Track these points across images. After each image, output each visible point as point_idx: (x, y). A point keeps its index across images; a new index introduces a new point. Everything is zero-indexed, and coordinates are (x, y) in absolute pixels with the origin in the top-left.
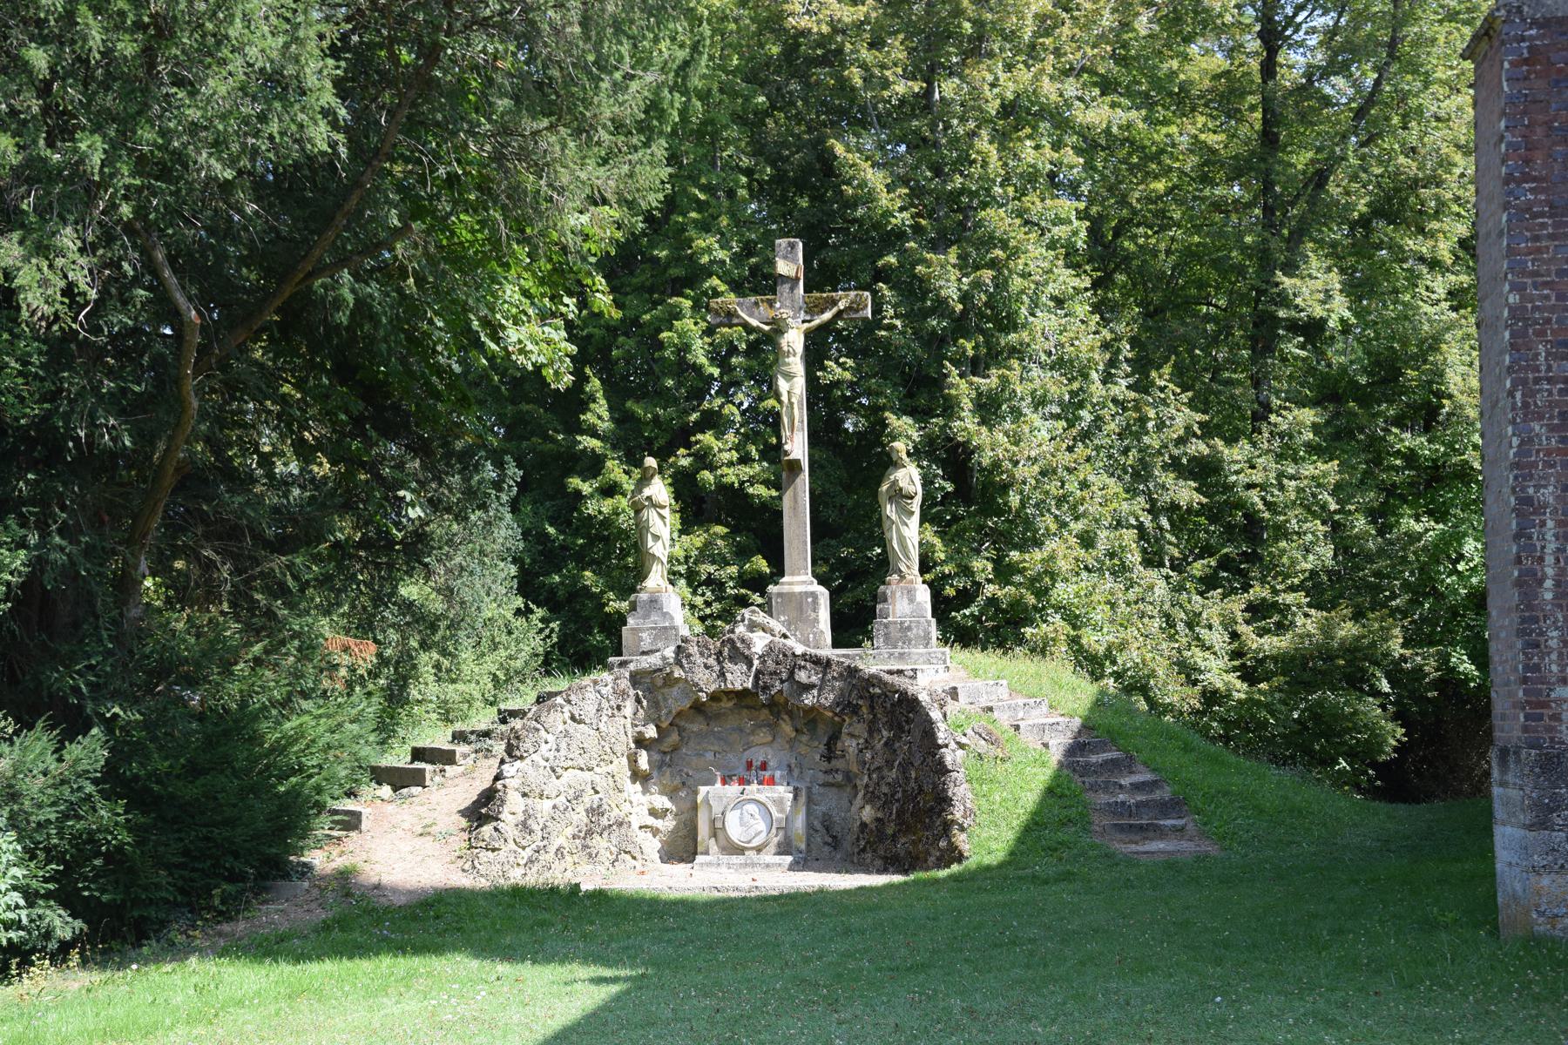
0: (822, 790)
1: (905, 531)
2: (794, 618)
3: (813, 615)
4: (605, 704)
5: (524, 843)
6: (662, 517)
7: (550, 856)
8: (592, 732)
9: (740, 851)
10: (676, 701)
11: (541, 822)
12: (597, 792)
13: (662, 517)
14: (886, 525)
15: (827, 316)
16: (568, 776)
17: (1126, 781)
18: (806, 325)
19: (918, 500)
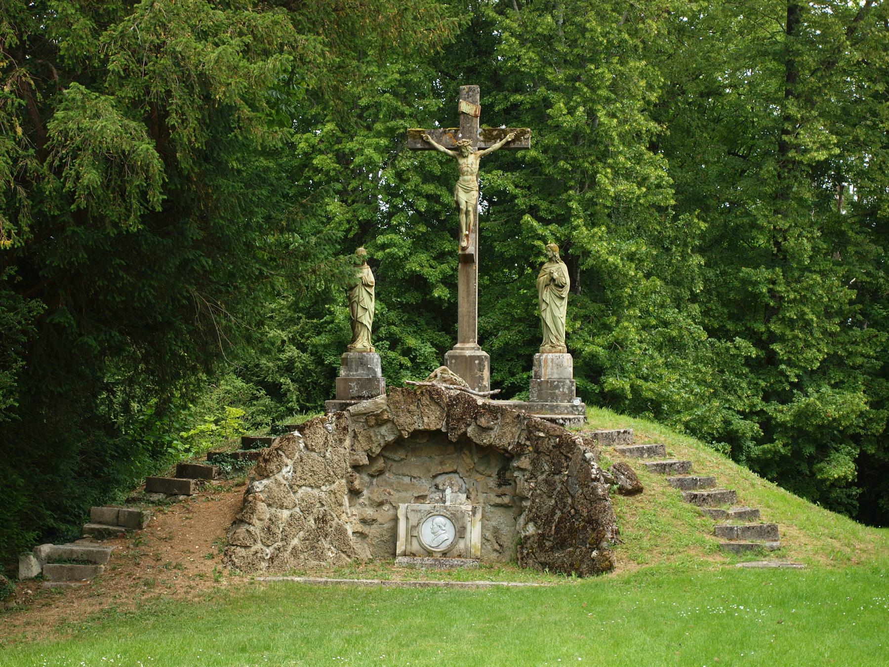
0: (493, 509)
1: (557, 314)
3: (479, 374)
4: (330, 438)
5: (268, 542)
7: (287, 554)
8: (320, 459)
9: (430, 553)
10: (387, 434)
11: (281, 526)
12: (323, 505)
14: (544, 306)
15: (497, 145)
16: (301, 492)
18: (482, 152)
19: (568, 288)
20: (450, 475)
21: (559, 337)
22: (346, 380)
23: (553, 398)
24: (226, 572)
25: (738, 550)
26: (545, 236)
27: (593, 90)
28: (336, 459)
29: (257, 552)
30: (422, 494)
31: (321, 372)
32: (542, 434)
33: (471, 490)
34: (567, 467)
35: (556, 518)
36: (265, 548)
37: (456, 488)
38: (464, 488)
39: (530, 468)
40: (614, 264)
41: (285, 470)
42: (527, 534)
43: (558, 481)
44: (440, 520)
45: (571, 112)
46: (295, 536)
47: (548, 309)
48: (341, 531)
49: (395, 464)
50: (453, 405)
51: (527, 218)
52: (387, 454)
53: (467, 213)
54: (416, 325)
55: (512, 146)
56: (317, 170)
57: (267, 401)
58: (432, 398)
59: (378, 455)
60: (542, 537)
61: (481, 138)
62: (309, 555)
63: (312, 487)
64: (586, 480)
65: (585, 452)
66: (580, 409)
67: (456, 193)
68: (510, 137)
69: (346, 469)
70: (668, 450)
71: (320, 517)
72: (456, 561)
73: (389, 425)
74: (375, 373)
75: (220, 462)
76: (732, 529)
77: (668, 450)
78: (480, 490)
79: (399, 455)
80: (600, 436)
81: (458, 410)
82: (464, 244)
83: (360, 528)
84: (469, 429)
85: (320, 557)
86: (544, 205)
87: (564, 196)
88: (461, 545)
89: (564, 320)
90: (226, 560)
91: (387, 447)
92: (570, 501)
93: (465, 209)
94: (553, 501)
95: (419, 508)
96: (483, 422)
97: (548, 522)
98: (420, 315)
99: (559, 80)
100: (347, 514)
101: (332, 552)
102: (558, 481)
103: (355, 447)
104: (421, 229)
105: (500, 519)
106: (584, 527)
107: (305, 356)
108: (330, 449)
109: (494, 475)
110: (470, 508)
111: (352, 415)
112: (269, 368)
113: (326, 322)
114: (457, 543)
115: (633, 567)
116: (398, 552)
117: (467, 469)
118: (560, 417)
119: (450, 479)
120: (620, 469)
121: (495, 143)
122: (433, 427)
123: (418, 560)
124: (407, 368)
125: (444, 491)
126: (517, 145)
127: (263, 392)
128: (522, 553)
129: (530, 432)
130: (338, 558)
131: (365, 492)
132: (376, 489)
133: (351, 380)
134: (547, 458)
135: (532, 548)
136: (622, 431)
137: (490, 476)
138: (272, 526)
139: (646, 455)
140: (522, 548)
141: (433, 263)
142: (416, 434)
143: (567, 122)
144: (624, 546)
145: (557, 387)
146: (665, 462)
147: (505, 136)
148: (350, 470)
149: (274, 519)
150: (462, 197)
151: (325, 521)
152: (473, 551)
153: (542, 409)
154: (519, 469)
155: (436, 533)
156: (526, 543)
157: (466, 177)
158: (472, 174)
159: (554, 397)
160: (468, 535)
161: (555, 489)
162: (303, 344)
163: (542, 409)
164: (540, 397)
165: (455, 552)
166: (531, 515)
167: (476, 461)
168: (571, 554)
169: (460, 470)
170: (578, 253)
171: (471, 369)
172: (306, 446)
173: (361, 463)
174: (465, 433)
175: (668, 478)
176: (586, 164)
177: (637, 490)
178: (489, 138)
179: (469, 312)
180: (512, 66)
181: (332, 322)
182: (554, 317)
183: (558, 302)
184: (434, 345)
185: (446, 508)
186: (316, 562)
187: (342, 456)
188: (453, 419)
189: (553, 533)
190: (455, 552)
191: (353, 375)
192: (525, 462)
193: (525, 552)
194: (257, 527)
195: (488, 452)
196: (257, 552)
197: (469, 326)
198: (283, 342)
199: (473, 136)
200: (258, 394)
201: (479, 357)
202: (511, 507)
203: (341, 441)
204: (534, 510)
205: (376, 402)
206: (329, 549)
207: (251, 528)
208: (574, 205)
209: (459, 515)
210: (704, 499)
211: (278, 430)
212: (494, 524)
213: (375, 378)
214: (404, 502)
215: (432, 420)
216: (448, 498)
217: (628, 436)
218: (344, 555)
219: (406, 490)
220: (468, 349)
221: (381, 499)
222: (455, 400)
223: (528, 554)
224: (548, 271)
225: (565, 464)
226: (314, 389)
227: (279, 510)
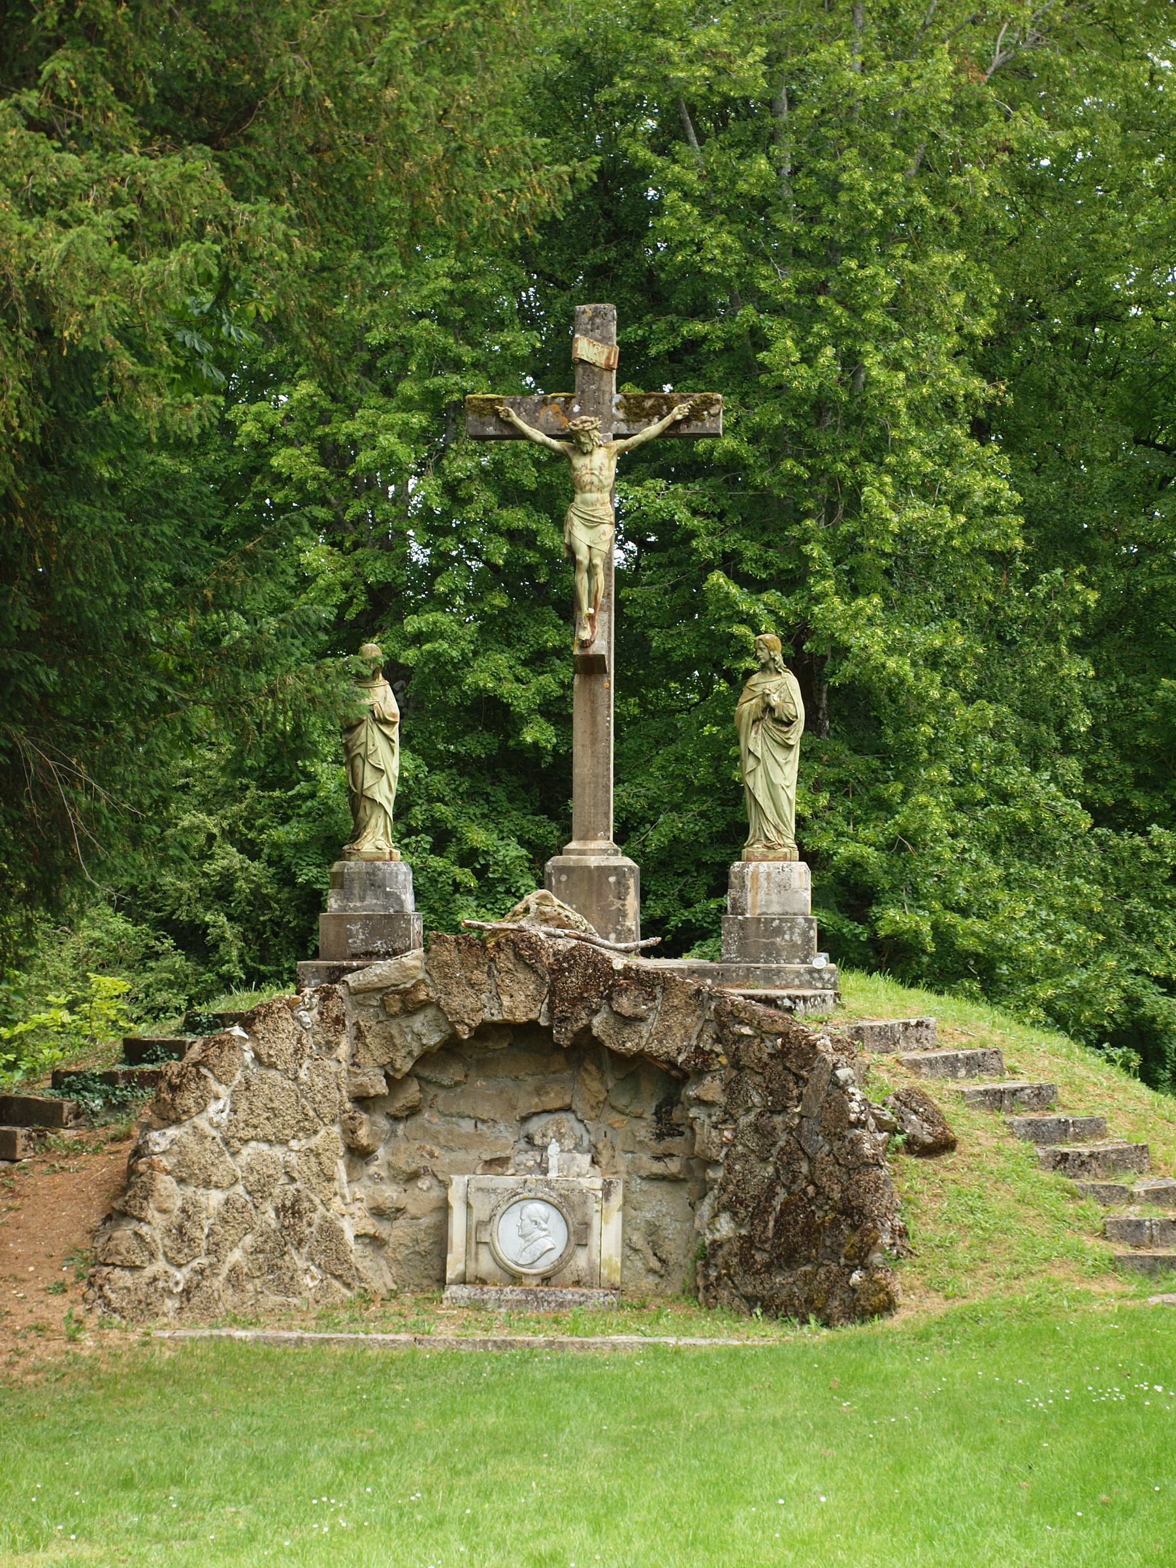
0: (645, 1186)
1: (778, 779)
2: (583, 902)
3: (618, 904)
4: (308, 1040)
5: (180, 1258)
6: (389, 739)
7: (218, 1283)
8: (288, 1084)
9: (515, 1278)
10: (424, 1031)
11: (206, 1224)
12: (293, 1180)
13: (389, 739)
14: (750, 763)
15: (654, 429)
17: (1140, 1187)
18: (621, 443)
20: (556, 1116)
21: (782, 827)
22: (341, 919)
23: (769, 954)
24: (92, 1321)
25: (1154, 1268)
26: (755, 615)
27: (855, 312)
28: (320, 1083)
29: (155, 1279)
30: (498, 1154)
31: (290, 900)
32: (746, 1031)
33: (600, 1146)
34: (800, 1098)
35: (777, 1204)
36: (172, 1270)
37: (569, 1143)
38: (586, 1143)
39: (722, 1099)
40: (896, 674)
41: (213, 1107)
42: (717, 1236)
43: (780, 1127)
45: (808, 358)
46: (234, 1244)
47: (760, 770)
48: (330, 1232)
49: (442, 1094)
50: (562, 970)
51: (717, 578)
52: (426, 1073)
53: (591, 570)
54: (488, 801)
55: (684, 430)
56: (279, 480)
57: (178, 960)
58: (518, 956)
59: (408, 1075)
60: (748, 1243)
61: (621, 414)
62: (264, 1283)
63: (269, 1142)
64: (839, 1123)
65: (835, 1067)
66: (826, 976)
67: (567, 528)
68: (679, 411)
69: (342, 1103)
70: (1008, 1062)
71: (288, 1203)
72: (569, 1294)
73: (430, 1013)
74: (401, 903)
75: (78, 1092)
76: (1139, 1225)
77: (1008, 1062)
78: (619, 1146)
79: (452, 1073)
80: (867, 1034)
81: (573, 981)
82: (585, 635)
83: (370, 1226)
84: (596, 1021)
85: (287, 1287)
86: (751, 550)
87: (794, 531)
88: (581, 1260)
89: (792, 793)
90: (91, 1294)
91: (427, 1058)
92: (805, 1168)
93: (586, 562)
94: (771, 1169)
95: (492, 1185)
96: (625, 1004)
97: (760, 1213)
98: (496, 780)
99: (783, 291)
100: (343, 1197)
101: (313, 1278)
102: (780, 1127)
103: (360, 1059)
104: (497, 602)
105: (661, 1205)
106: (835, 1223)
107: (256, 867)
108: (307, 1063)
109: (649, 1116)
110: (598, 1183)
111: (354, 992)
112: (181, 892)
113: (299, 796)
114: (572, 1256)
115: (937, 1306)
116: (450, 1275)
117: (593, 1102)
118: (784, 993)
119: (558, 1124)
120: (908, 1101)
121: (649, 424)
122: (521, 1017)
123: (491, 1292)
124: (469, 891)
125: (544, 1148)
126: (694, 428)
127: (169, 942)
128: (706, 1276)
129: (722, 1026)
130: (325, 1290)
131: (381, 1152)
132: (403, 1146)
133: (351, 919)
134: (758, 1079)
135: (727, 1266)
136: (913, 1022)
137: (639, 1117)
138: (188, 1225)
139: (962, 1072)
140: (707, 1265)
141: (521, 671)
142: (486, 1031)
143: (801, 379)
144: (918, 1262)
145: (779, 931)
146: (1001, 1086)
147: (670, 409)
148: (348, 1106)
149: (191, 1210)
150: (581, 536)
151: (297, 1213)
152: (605, 1272)
153: (747, 977)
154: (700, 1102)
155: (529, 1235)
156: (714, 1256)
157: (588, 496)
158: (600, 490)
159: (772, 952)
160: (594, 1240)
161: (774, 1144)
162: (252, 842)
163: (747, 977)
164: (743, 952)
166: (725, 1198)
167: (610, 1085)
168: (807, 1279)
169: (578, 1105)
170: (824, 649)
171: (601, 895)
172: (258, 1058)
173: (372, 1092)
174: (588, 1028)
175: (1009, 1119)
176: (840, 466)
177: (943, 1146)
178: (636, 413)
179: (596, 776)
180: (685, 262)
181: (312, 795)
182: (771, 785)
183: (780, 755)
184: (522, 842)
185: (548, 1184)
186: (280, 1299)
187: (331, 1078)
188: (562, 1000)
189: (770, 1234)
190: (568, 1275)
191: (355, 909)
192: (711, 1088)
193: (713, 1274)
194: (155, 1227)
195: (635, 1068)
196: (155, 1279)
197: (595, 805)
198: (211, 837)
199: (604, 410)
200: (159, 947)
201: (616, 870)
202: (684, 1180)
203: (330, 1046)
204: (731, 1188)
205: (402, 965)
206: (306, 1271)
207: (144, 1229)
208: (814, 550)
209: (575, 1198)
210: (1083, 1163)
211: (199, 1024)
212: (648, 1216)
213: (401, 914)
214: (461, 1172)
215: (519, 1001)
216: (553, 1162)
217: (926, 1033)
218: (337, 1284)
219: (466, 1148)
220: (594, 852)
221: (414, 1167)
222: (566, 959)
223: (718, 1278)
224: (758, 690)
225: (795, 1092)
226: (276, 935)
227: (201, 1190)
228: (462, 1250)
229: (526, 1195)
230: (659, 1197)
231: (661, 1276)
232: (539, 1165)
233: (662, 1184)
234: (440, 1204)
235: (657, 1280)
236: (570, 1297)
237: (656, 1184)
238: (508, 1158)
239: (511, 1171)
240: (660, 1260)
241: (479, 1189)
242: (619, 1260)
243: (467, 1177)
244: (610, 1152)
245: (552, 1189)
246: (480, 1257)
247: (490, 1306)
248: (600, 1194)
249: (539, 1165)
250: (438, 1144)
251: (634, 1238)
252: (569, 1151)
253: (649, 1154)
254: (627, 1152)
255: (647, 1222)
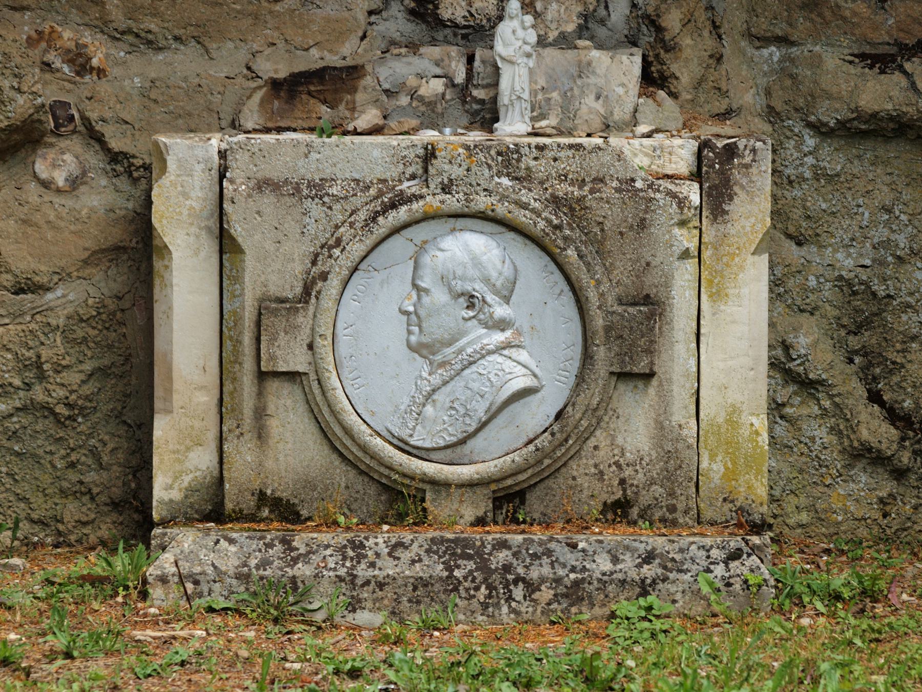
0: (834, 159)
9: (399, 499)
30: (314, 59)
44: (470, 250)
72: (602, 553)
88: (632, 430)
95: (309, 169)
110: (680, 154)
114: (599, 415)
116: (166, 489)
123: (320, 553)
152: (714, 468)
155: (440, 344)
160: (677, 357)
165: (586, 482)
185: (508, 159)
190: (586, 482)
209: (609, 210)
212: (846, 262)
214: (190, 124)
216: (515, 82)
228: (206, 400)
229: (434, 201)
230: (884, 195)
231: (899, 474)
232: (463, 91)
233: (890, 151)
234: (116, 235)
235: (887, 487)
236: (604, 564)
237: (869, 150)
238: (354, 72)
239: (369, 117)
240: (893, 415)
241: (263, 185)
242: (760, 423)
243: (215, 142)
244: (709, 42)
245: (524, 179)
246: (273, 425)
247: (319, 603)
248: (693, 193)
249: (463, 91)
250: (103, 26)
251: (802, 342)
252: (564, 42)
253: (847, 45)
254: (764, 41)
255: (844, 284)
